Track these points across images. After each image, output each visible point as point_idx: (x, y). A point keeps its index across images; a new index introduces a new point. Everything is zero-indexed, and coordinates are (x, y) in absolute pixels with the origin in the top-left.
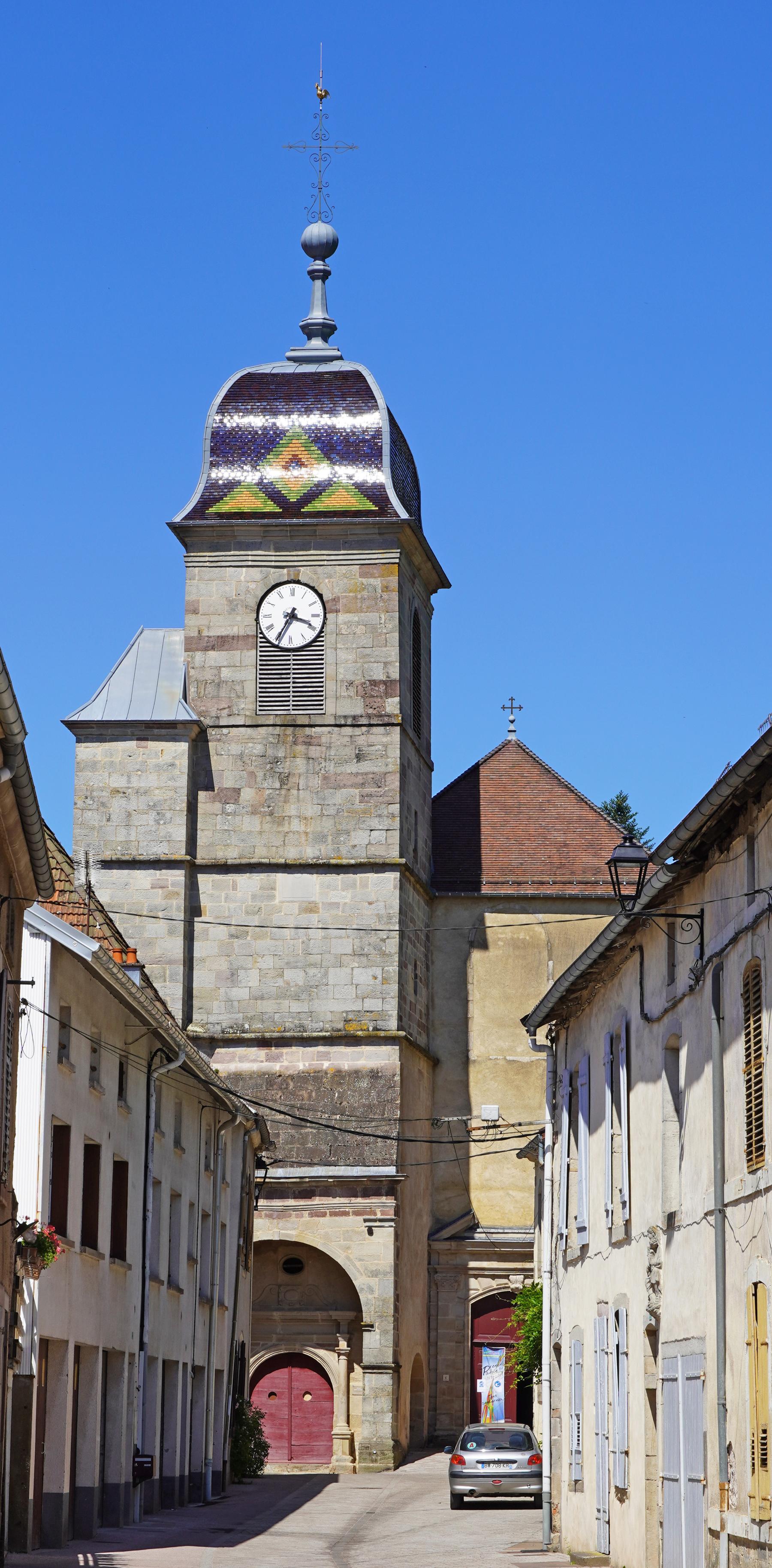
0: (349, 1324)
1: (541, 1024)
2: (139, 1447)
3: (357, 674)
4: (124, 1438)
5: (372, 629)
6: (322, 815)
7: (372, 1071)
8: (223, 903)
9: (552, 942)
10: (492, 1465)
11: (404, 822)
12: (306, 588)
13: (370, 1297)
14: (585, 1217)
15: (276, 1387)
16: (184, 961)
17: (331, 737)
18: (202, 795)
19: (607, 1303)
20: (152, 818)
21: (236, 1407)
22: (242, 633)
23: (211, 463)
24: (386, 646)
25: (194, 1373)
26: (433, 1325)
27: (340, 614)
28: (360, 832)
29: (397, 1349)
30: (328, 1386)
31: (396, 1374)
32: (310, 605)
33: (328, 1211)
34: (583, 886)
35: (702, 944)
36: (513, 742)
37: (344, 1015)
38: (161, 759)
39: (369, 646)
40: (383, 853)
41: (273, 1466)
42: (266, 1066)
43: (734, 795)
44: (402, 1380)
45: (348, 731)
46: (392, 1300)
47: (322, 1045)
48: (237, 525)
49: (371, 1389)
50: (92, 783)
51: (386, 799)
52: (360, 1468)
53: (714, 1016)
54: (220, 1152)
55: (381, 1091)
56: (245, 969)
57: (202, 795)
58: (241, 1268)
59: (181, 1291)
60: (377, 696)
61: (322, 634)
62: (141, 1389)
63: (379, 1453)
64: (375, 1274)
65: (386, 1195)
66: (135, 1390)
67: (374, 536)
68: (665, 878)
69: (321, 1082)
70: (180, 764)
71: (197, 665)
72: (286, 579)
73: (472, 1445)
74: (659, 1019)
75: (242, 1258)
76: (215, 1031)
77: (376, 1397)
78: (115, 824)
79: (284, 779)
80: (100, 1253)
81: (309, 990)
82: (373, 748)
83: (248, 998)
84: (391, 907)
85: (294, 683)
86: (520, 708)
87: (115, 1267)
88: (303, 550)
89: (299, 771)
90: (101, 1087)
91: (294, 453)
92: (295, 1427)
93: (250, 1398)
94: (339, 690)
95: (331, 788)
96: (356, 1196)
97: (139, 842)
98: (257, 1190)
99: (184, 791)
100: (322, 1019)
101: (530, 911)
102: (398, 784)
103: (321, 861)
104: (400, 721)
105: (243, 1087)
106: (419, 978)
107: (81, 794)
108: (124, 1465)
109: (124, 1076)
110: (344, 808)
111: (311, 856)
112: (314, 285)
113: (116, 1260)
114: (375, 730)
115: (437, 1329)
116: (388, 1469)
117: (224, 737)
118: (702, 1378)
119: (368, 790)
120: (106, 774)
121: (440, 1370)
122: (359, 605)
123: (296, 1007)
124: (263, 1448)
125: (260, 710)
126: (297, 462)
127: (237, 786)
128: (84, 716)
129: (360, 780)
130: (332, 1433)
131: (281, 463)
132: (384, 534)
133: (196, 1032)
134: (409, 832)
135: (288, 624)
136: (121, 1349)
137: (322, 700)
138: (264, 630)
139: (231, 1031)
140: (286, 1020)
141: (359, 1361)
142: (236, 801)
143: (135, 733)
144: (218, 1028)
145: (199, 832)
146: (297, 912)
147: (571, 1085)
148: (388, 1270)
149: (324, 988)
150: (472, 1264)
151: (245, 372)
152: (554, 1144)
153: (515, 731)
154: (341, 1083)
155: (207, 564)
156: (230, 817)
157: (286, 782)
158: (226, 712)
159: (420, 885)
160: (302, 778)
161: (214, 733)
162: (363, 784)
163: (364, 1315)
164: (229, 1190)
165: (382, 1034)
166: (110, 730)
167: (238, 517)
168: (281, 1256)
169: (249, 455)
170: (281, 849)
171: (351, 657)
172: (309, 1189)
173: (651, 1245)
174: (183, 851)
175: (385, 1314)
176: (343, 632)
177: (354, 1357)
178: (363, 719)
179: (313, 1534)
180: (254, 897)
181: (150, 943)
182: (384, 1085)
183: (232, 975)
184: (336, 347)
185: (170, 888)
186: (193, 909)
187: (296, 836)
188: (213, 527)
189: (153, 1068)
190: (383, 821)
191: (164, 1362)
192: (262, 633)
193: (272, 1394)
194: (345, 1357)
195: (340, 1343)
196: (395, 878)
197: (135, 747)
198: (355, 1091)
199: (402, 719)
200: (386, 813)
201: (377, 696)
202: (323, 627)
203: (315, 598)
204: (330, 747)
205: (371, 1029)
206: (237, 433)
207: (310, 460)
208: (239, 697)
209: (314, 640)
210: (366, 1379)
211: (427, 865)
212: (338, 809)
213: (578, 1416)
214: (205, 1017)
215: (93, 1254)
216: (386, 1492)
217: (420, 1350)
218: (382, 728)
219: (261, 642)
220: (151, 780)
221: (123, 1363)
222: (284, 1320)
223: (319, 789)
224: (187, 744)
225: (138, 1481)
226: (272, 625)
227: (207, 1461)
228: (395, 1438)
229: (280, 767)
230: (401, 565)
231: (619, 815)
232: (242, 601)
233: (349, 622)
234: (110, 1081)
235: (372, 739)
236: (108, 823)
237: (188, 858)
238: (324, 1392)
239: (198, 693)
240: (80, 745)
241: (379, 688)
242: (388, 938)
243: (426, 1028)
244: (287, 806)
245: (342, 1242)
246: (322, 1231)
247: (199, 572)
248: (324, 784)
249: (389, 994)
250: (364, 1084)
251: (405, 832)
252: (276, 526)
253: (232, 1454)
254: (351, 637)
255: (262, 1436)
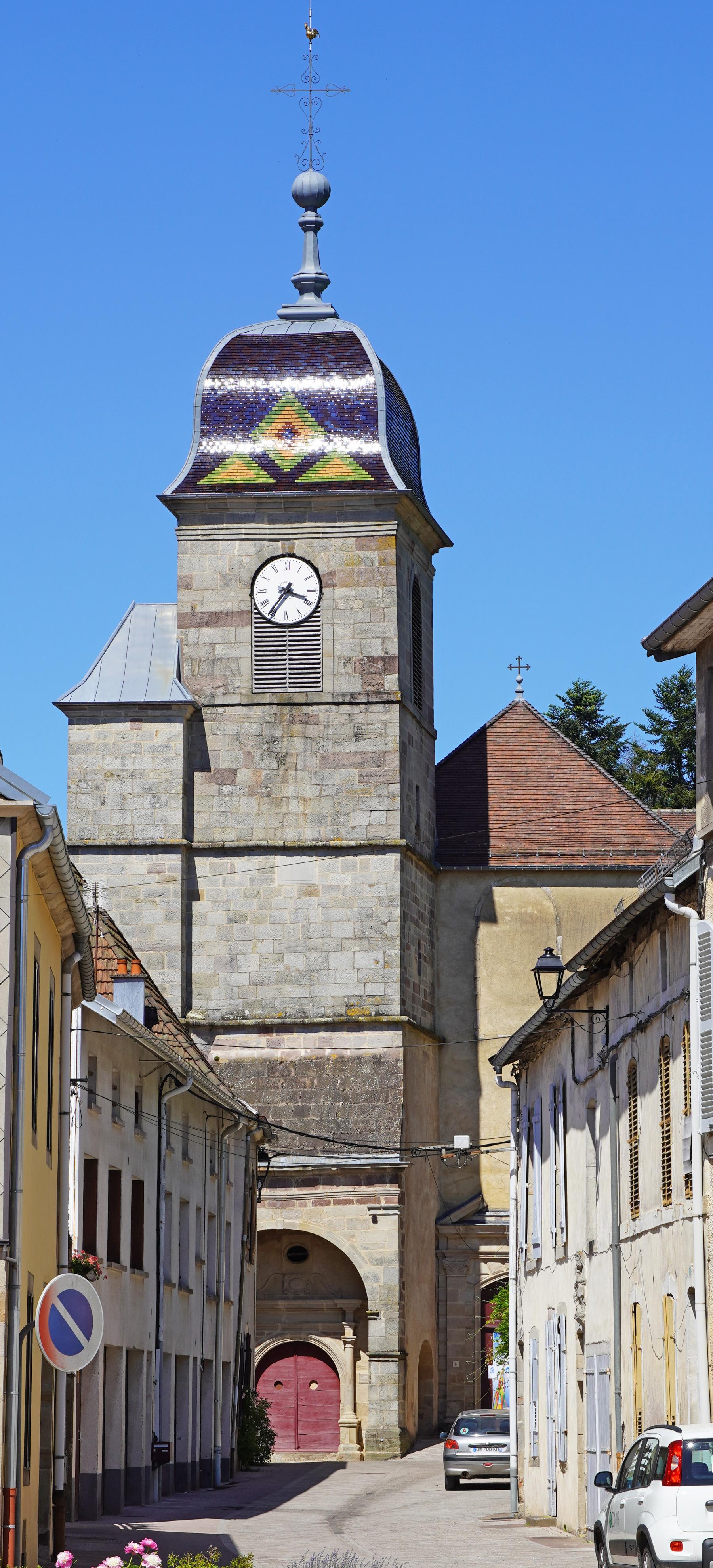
0: (355, 1312)
1: (505, 1064)
2: (157, 1435)
3: (355, 651)
4: (144, 1427)
5: (370, 604)
6: (321, 796)
7: (375, 1057)
8: (221, 887)
9: (561, 917)
10: (483, 1449)
11: (405, 799)
12: (302, 562)
13: (375, 1285)
14: (539, 1236)
15: (282, 1376)
16: (182, 947)
17: (329, 716)
18: (198, 776)
19: (553, 1309)
20: (147, 801)
21: (243, 1397)
22: (236, 609)
23: (202, 431)
24: (384, 621)
25: (203, 1366)
26: (442, 1311)
27: (336, 588)
28: (360, 813)
29: (404, 1336)
30: (334, 1375)
31: (403, 1362)
32: (306, 579)
33: (332, 1200)
34: (592, 858)
35: (607, 1034)
36: (521, 704)
37: (346, 999)
38: (155, 741)
39: (366, 621)
40: (384, 835)
41: (280, 1455)
42: (267, 1053)
43: (617, 937)
44: (410, 1368)
45: (346, 709)
46: (397, 1288)
47: (324, 1031)
48: (230, 498)
49: (378, 1377)
50: (86, 766)
51: (385, 779)
52: (368, 1456)
53: (612, 1096)
54: (224, 1156)
55: (384, 1078)
56: (245, 954)
57: (198, 776)
58: (246, 1264)
59: (190, 1291)
60: (375, 673)
61: (319, 610)
62: (158, 1383)
63: (386, 1440)
64: (379, 1262)
65: (391, 1183)
66: (153, 1384)
67: (371, 507)
68: (578, 981)
69: (324, 1068)
70: (175, 746)
71: (191, 642)
72: (280, 553)
73: (465, 1431)
74: (584, 1083)
75: (247, 1252)
76: (215, 1017)
77: (382, 1385)
78: (110, 808)
79: (281, 760)
80: (123, 1266)
81: (310, 975)
82: (372, 726)
83: (247, 983)
84: (392, 890)
85: (290, 659)
86: (528, 667)
87: (134, 1276)
88: (297, 522)
89: (297, 751)
90: (122, 1121)
91: (287, 420)
92: (302, 1416)
93: (256, 1388)
94: (336, 667)
95: (329, 768)
96: (360, 1184)
97: (134, 826)
98: (260, 1183)
99: (180, 773)
100: (323, 1004)
101: (538, 885)
102: (397, 763)
103: (320, 844)
104: (399, 699)
105: (244, 1074)
106: (422, 957)
107: (75, 777)
108: (144, 1450)
109: (139, 1105)
110: (343, 788)
111: (310, 837)
112: (306, 237)
113: (136, 1270)
114: (374, 707)
115: (446, 1315)
116: (395, 1457)
117: (219, 716)
118: (608, 1373)
119: (368, 769)
120: (100, 756)
121: (450, 1355)
122: (356, 579)
123: (296, 992)
124: (270, 1437)
125: (256, 688)
126: (289, 431)
127: (233, 767)
128: (76, 698)
129: (359, 759)
130: (339, 1421)
131: (274, 431)
132: (380, 505)
133: (196, 1018)
134: (410, 810)
135: (282, 599)
136: (141, 1348)
137: (319, 678)
138: (258, 605)
139: (231, 1017)
140: (287, 1005)
141: (366, 1350)
142: (233, 782)
143: (129, 715)
144: (218, 1014)
145: (196, 815)
146: (296, 895)
147: (529, 1120)
148: (393, 1257)
149: (325, 972)
150: (484, 1248)
151: (235, 334)
152: (518, 1168)
153: (522, 692)
154: (343, 1070)
155: (200, 538)
156: (227, 799)
157: (284, 762)
158: (221, 690)
159: (423, 862)
160: (300, 757)
161: (209, 712)
162: (362, 763)
163: (369, 1303)
164: (232, 1189)
165: (385, 1019)
166: (102, 712)
167: (230, 490)
168: (286, 1244)
169: (241, 423)
170: (279, 832)
171: (348, 633)
172: (312, 1177)
173: (578, 1266)
174: (180, 835)
175: (391, 1302)
176: (340, 607)
177: (360, 1345)
178: (361, 696)
179: (315, 1510)
180: (252, 880)
181: (147, 929)
182: (388, 1071)
183: (232, 960)
184: (329, 304)
185: (167, 873)
186: (191, 894)
187: (295, 817)
188: (205, 499)
189: (163, 1093)
190: (383, 802)
191: (176, 1356)
192: (256, 608)
193: (278, 1383)
194: (351, 1346)
195: (346, 1331)
196: (396, 860)
197: (129, 729)
198: (358, 1077)
199: (402, 696)
200: (386, 793)
201: (375, 673)
202: (319, 602)
203: (311, 572)
204: (328, 726)
205: (373, 1014)
206: (228, 400)
207: (304, 427)
208: (234, 675)
209: (311, 616)
210: (372, 1367)
211: (431, 838)
212: (337, 789)
213: (535, 1403)
214: (204, 1003)
215: (117, 1268)
216: (389, 1477)
217: (428, 1337)
218: (382, 705)
219: (256, 618)
220: (145, 763)
221: (142, 1360)
222: (289, 1309)
223: (318, 769)
224: (182, 725)
225: (156, 1465)
226: (267, 601)
227: (216, 1449)
228: (402, 1426)
229: (277, 746)
230: (399, 536)
231: (682, 693)
232: (235, 575)
233: (346, 596)
234: (128, 1117)
235: (371, 717)
236: (103, 807)
237: (185, 842)
238: (330, 1381)
239: (192, 671)
240: (72, 726)
241: (378, 664)
242: (389, 921)
243: (431, 1008)
244: (284, 787)
245: (346, 1231)
246: (326, 1220)
247: (191, 546)
248: (322, 764)
249: (391, 978)
250: (367, 1070)
251: (406, 810)
252: (270, 498)
253: (239, 1443)
254: (348, 612)
255: (268, 1424)
